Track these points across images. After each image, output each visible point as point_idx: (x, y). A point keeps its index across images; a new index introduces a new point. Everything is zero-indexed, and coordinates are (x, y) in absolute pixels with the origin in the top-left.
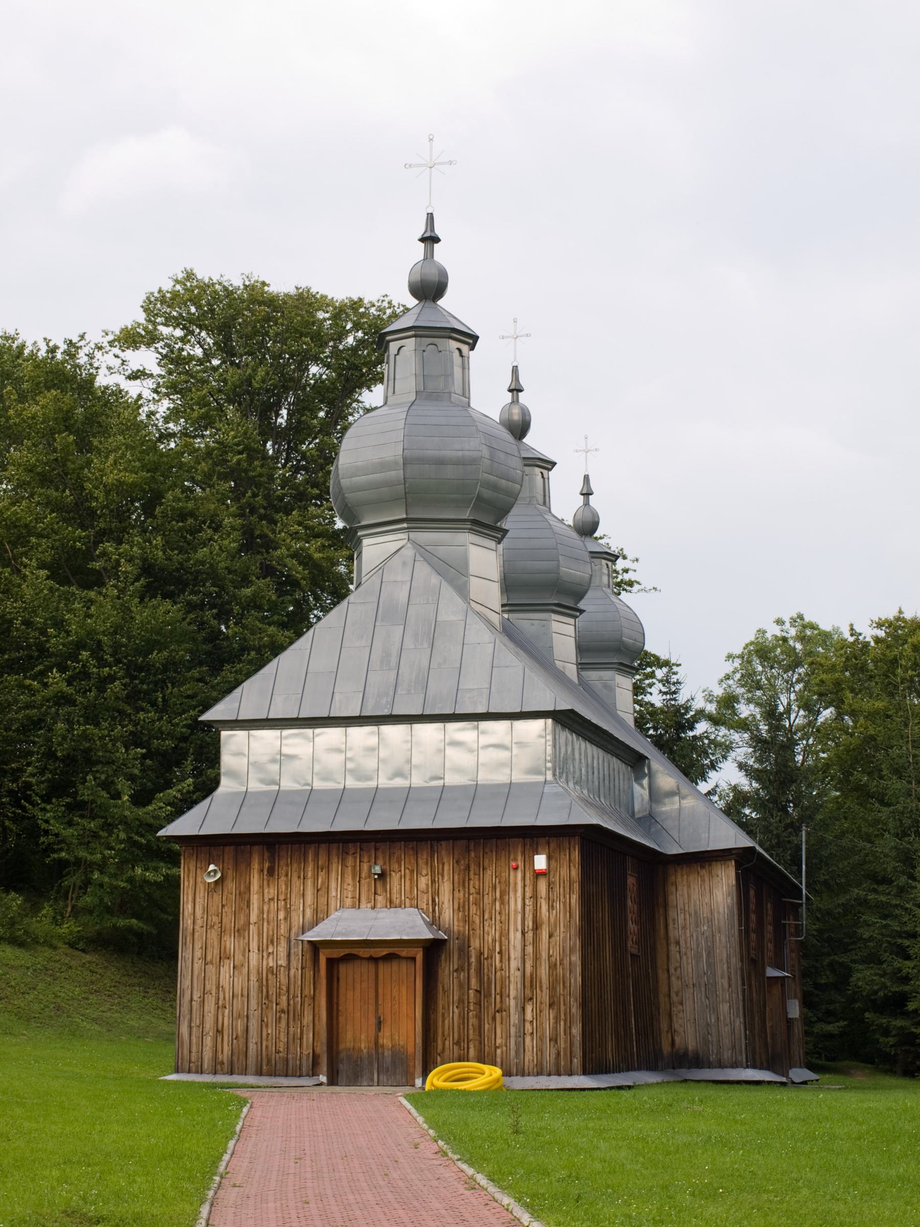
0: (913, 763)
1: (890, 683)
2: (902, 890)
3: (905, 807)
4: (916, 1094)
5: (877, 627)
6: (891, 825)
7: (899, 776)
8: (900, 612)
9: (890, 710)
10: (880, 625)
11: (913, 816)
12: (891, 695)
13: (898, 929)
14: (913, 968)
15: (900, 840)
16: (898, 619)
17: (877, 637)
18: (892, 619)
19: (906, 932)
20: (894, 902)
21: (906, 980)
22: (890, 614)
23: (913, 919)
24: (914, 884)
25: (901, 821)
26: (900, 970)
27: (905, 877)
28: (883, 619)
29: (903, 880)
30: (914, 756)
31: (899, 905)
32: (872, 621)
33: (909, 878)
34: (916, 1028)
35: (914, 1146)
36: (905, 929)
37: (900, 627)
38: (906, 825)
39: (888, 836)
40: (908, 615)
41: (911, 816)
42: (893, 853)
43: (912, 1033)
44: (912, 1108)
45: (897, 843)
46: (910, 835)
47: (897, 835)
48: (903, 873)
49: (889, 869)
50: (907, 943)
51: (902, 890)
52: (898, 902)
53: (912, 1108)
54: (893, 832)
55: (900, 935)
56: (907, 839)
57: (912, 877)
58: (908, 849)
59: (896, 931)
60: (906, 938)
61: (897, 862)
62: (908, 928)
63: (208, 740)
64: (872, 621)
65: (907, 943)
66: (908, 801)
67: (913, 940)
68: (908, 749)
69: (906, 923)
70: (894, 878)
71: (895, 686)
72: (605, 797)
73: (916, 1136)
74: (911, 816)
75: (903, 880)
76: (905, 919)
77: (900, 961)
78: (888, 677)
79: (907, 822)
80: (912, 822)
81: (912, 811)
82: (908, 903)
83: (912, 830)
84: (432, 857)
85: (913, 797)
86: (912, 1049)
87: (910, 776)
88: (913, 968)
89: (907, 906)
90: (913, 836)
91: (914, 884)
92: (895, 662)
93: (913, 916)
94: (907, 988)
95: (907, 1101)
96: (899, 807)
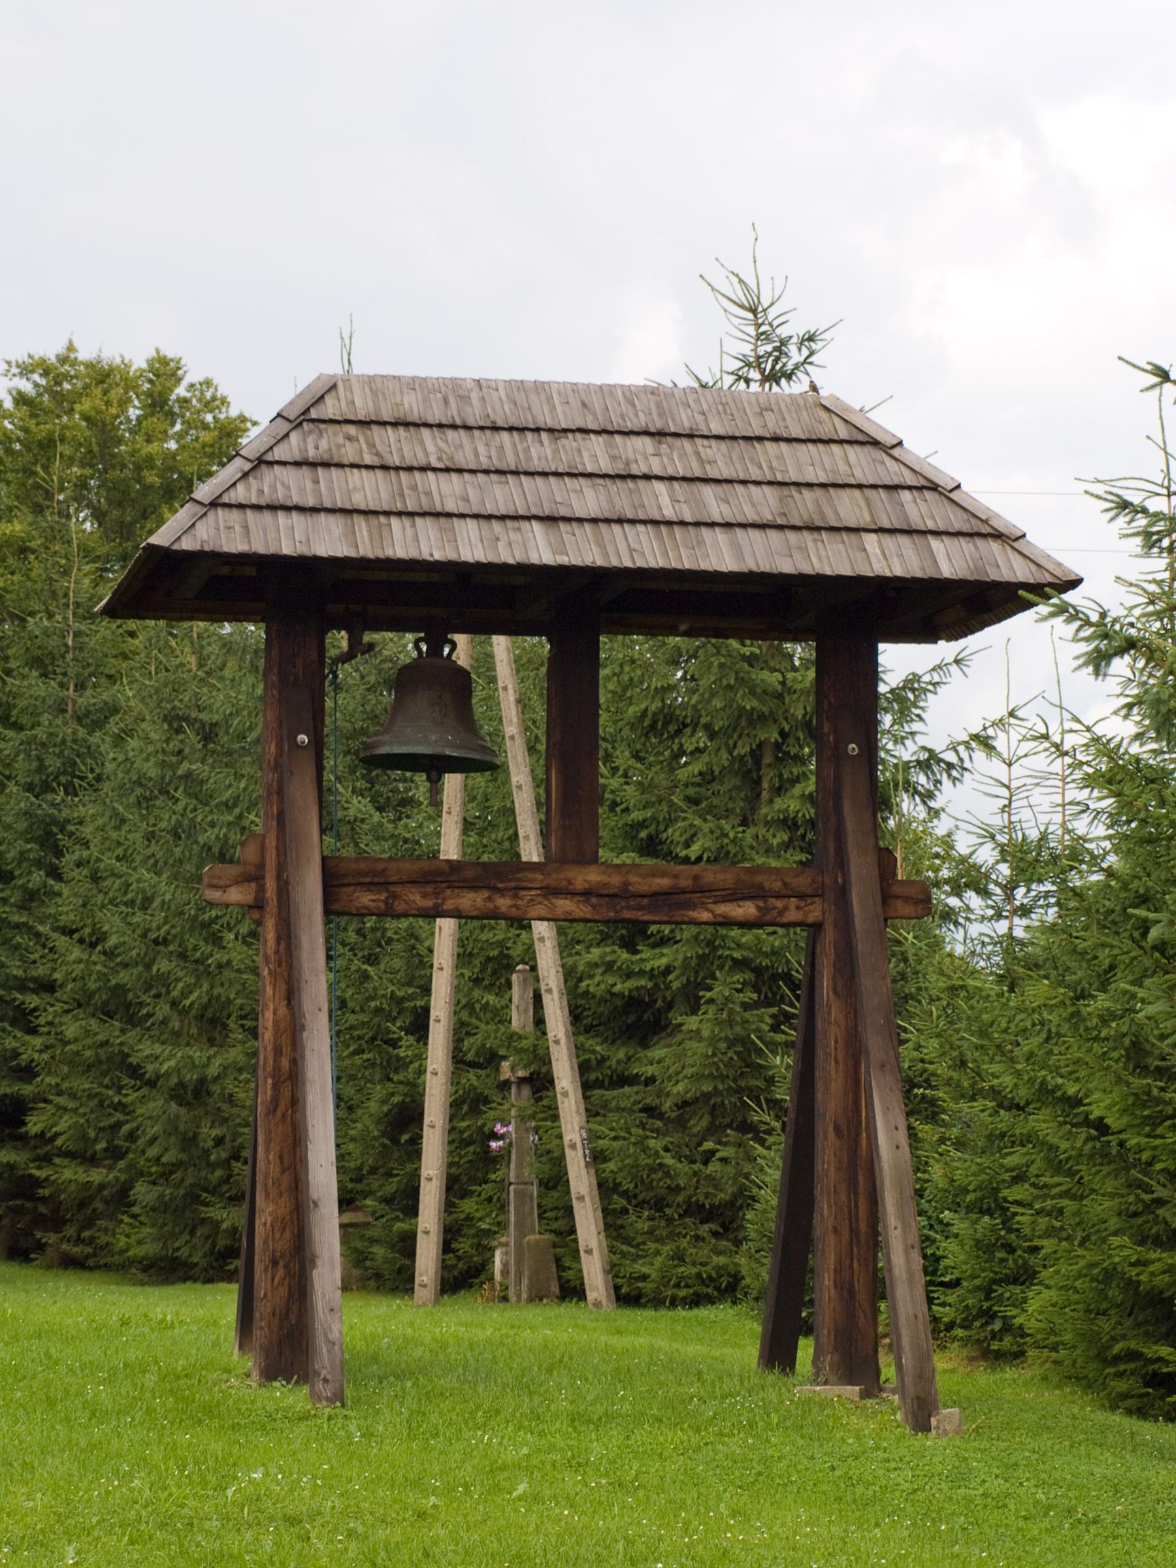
0: (74, 648)
1: (37, 486)
2: (31, 898)
3: (51, 734)
4: (27, 1292)
5: (21, 373)
6: (22, 765)
7: (42, 671)
8: (71, 348)
9: (33, 538)
10: (25, 370)
11: (66, 753)
12: (38, 510)
13: (20, 973)
14: (41, 1051)
15: (37, 797)
16: (63, 360)
17: (20, 393)
18: (53, 359)
19: (34, 979)
20: (15, 918)
21: (28, 1073)
22: (50, 350)
23: (51, 956)
24: (57, 887)
25: (40, 759)
26: (16, 1054)
27: (42, 873)
28: (36, 358)
29: (37, 878)
30: (77, 634)
31: (25, 924)
32: (9, 363)
33: (48, 875)
34: (39, 1168)
35: (12, 1390)
36: (34, 973)
37: (67, 377)
38: (50, 770)
39: (15, 789)
40: (85, 354)
41: (62, 752)
42: (22, 825)
43: (31, 1176)
44: (14, 1318)
45: (32, 804)
46: (53, 791)
47: (29, 788)
48: (38, 863)
49: (10, 856)
50: (33, 1001)
51: (31, 898)
52: (24, 919)
53: (14, 1318)
54: (23, 781)
55: (22, 985)
56: (49, 797)
57: (55, 873)
58: (52, 816)
59: (16, 977)
60: (35, 991)
61: (27, 841)
62: (40, 971)
63: (1138, 1112)
64: (9, 363)
65: (33, 1001)
66: (59, 721)
67: (47, 997)
68: (65, 619)
69: (34, 962)
70: (17, 873)
71: (47, 491)
72: (267, 1195)
73: (17, 1371)
74: (62, 752)
75: (37, 878)
76: (35, 956)
77: (19, 1034)
78: (34, 474)
79: (53, 763)
80: (64, 764)
81: (64, 741)
82: (41, 923)
83: (63, 779)
84: (975, 567)
85: (68, 716)
86: (29, 1205)
87: (65, 674)
88: (41, 1051)
89: (41, 928)
90: (62, 793)
91: (57, 887)
92: (48, 445)
93: (51, 950)
94: (28, 1089)
95: (6, 1305)
96: (41, 733)
